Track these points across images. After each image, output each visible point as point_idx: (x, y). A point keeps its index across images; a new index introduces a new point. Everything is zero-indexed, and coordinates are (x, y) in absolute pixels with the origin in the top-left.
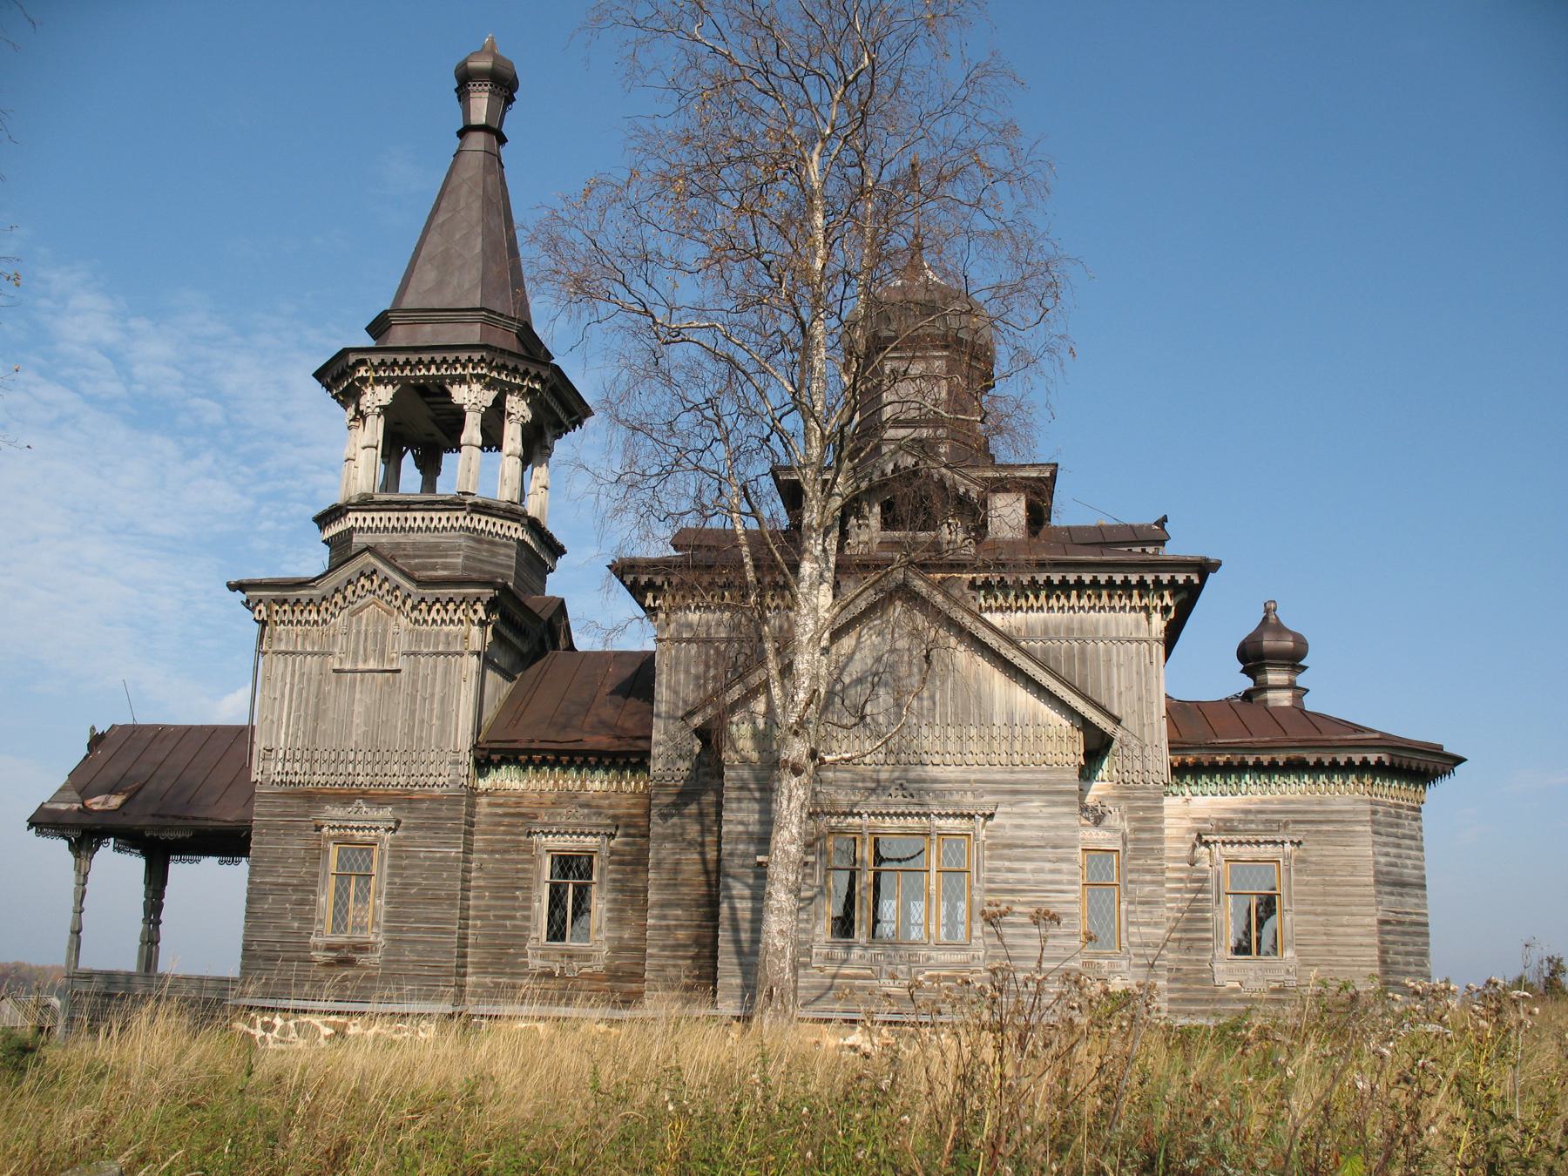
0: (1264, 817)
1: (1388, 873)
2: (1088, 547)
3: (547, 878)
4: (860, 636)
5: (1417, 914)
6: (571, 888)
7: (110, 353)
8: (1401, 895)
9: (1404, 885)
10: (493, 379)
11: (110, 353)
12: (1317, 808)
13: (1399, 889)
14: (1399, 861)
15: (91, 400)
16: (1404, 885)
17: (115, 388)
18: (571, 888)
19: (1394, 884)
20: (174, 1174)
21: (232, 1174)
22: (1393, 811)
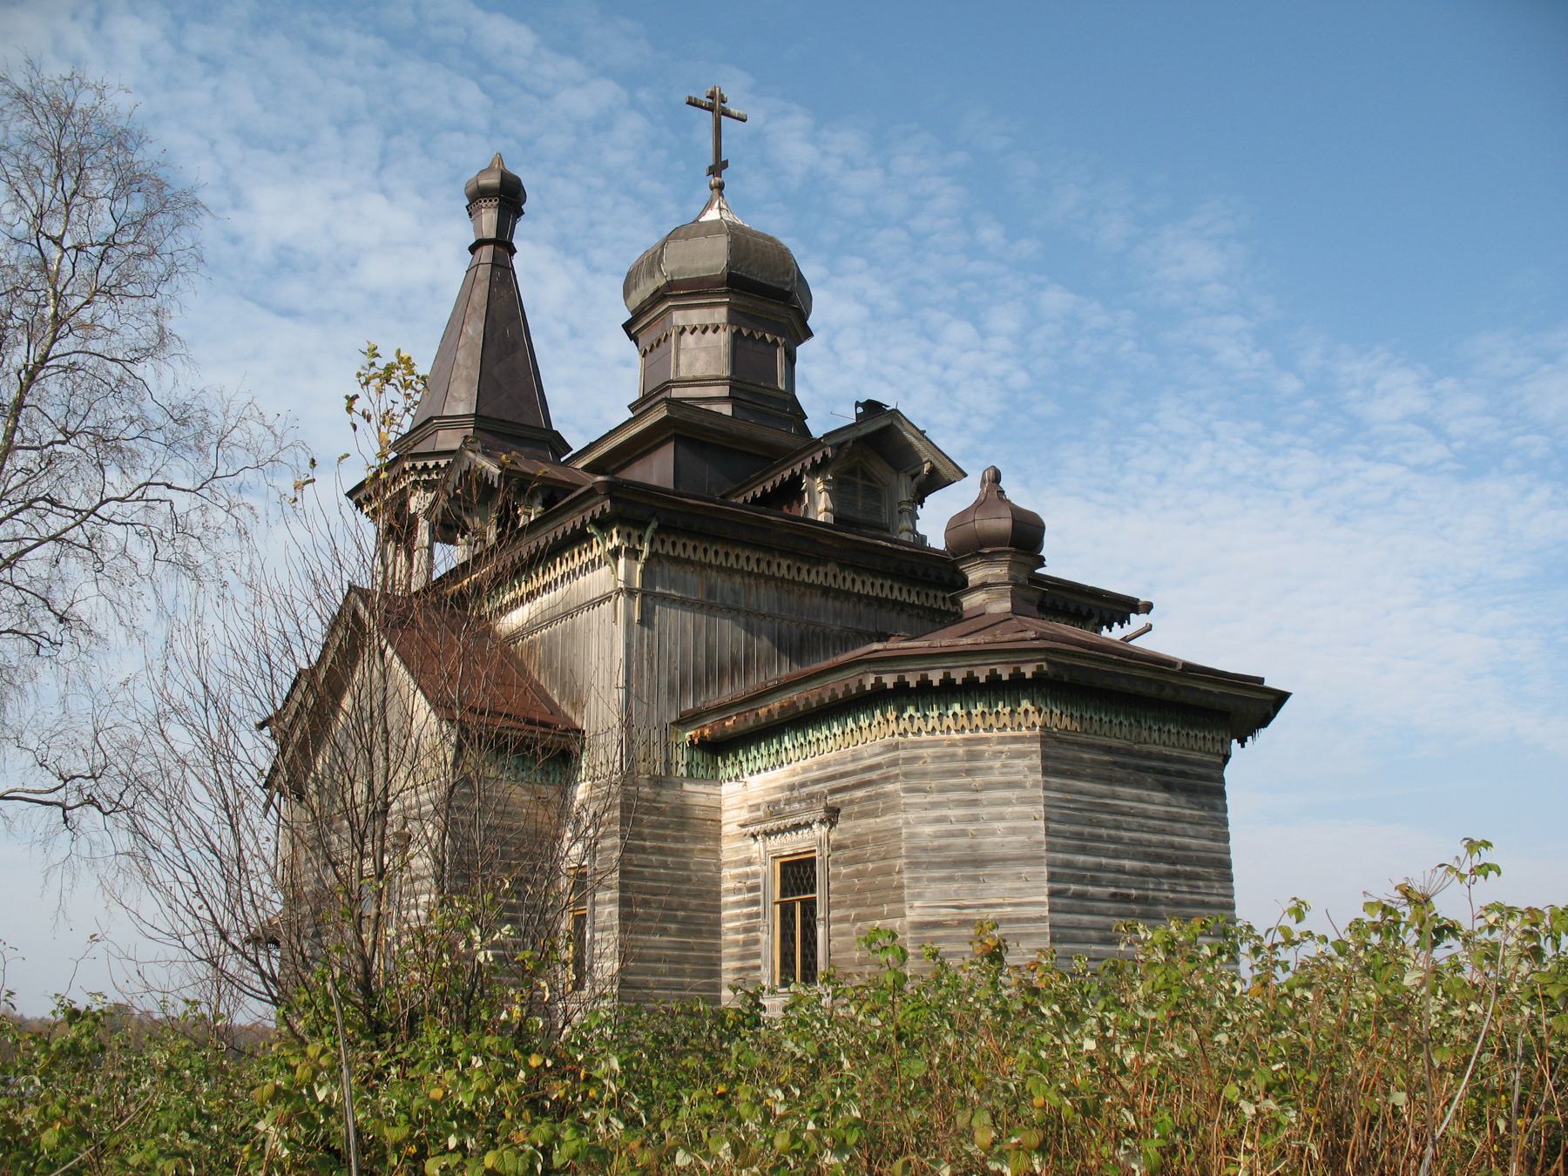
0: (805, 791)
1: (939, 849)
2: (567, 512)
3: (777, 897)
4: (309, 662)
5: (1010, 905)
6: (798, 906)
7: (1423, 421)
8: (975, 878)
9: (980, 862)
10: (425, 481)
11: (1423, 421)
12: (850, 767)
13: (970, 871)
14: (971, 828)
15: (1418, 469)
16: (980, 862)
17: (1436, 451)
18: (798, 906)
19: (957, 863)
20: (432, 1167)
21: (548, 1173)
22: (960, 751)
